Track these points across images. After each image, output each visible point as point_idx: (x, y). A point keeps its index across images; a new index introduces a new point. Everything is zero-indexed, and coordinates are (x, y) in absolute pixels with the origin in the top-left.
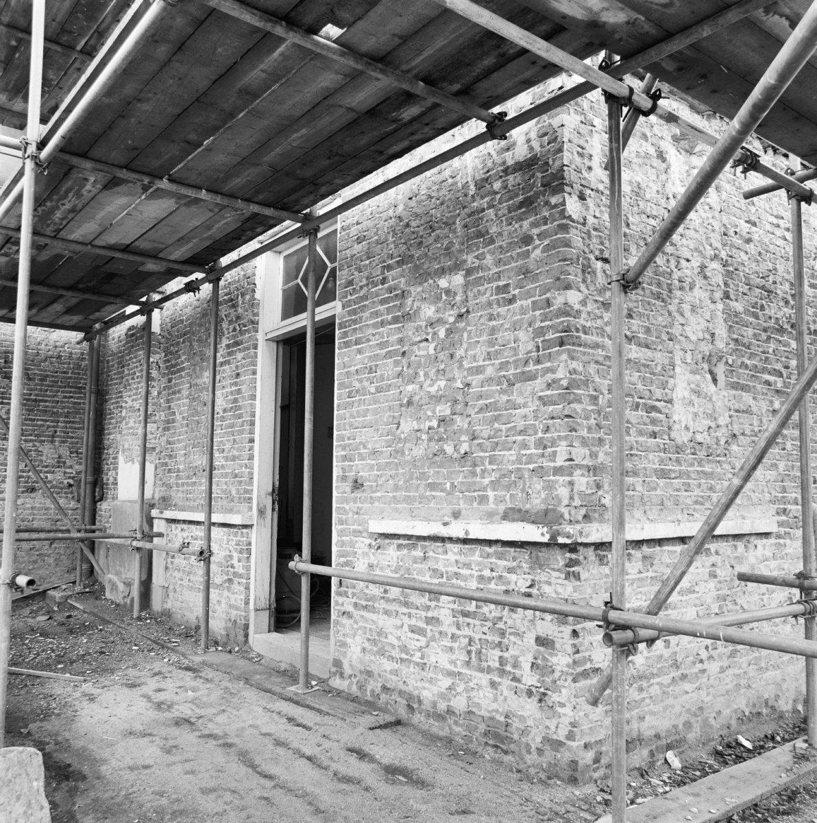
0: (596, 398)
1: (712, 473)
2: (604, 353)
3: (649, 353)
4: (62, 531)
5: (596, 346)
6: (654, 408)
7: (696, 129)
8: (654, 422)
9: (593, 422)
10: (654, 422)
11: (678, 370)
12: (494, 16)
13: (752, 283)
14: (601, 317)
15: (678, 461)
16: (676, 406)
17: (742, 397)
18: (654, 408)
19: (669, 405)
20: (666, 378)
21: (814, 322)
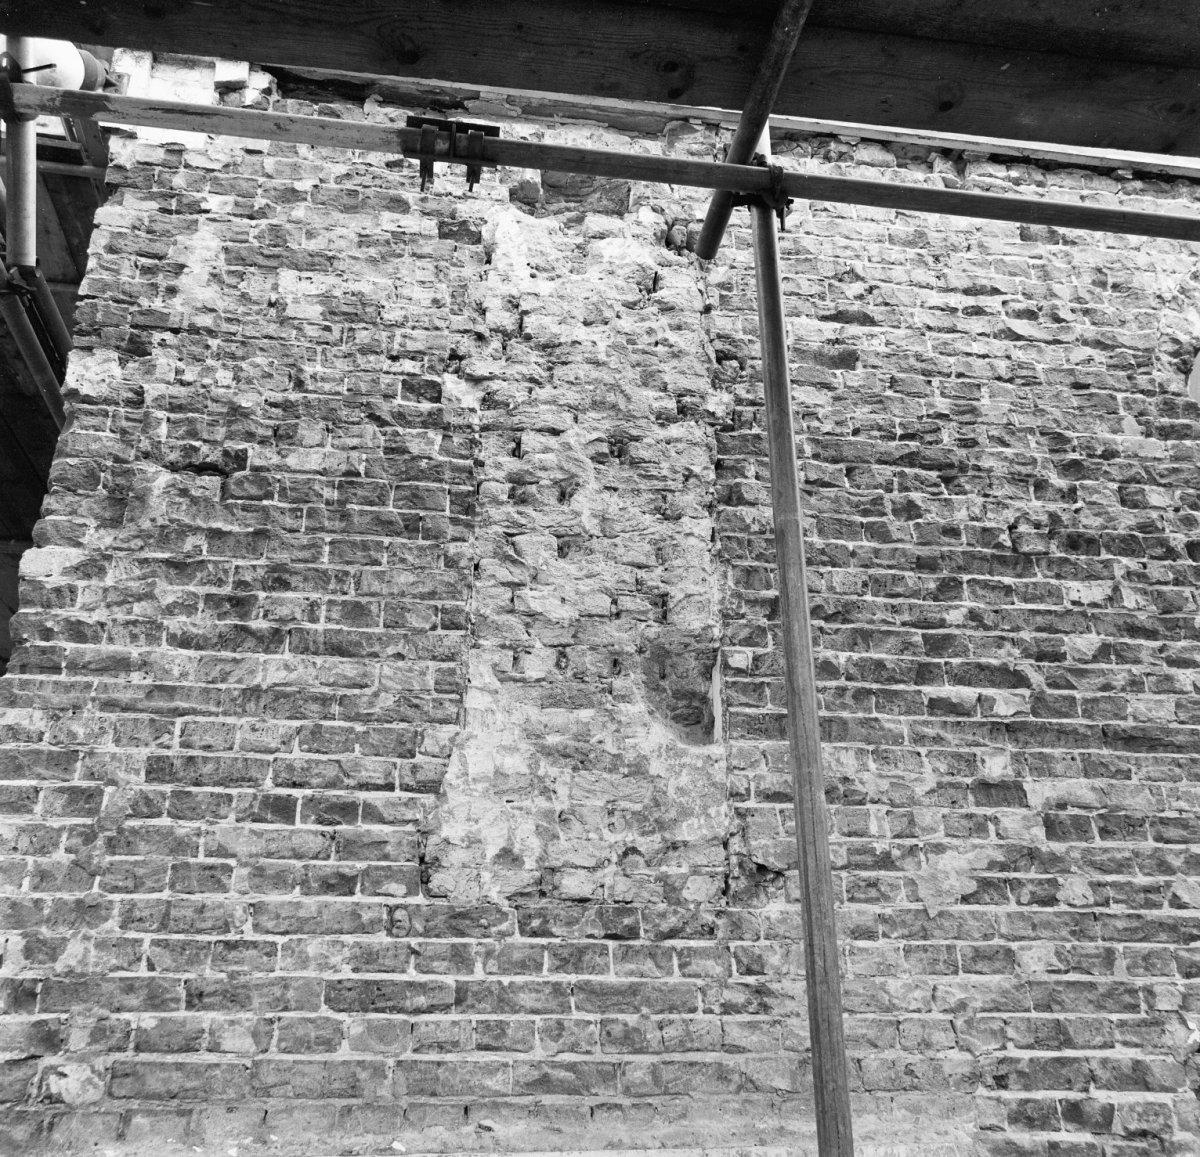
0: (93, 795)
1: (634, 990)
2: (149, 681)
3: (347, 668)
4: (1038, 612)
5: (121, 664)
6: (348, 811)
7: (201, 114)
8: (349, 848)
9: (61, 856)
10: (349, 848)
11: (474, 700)
12: (859, 207)
13: (848, 452)
14: (149, 596)
15: (460, 959)
16: (455, 798)
17: (992, 701)
18: (348, 811)
19: (428, 799)
20: (419, 726)
21: (1189, 522)
